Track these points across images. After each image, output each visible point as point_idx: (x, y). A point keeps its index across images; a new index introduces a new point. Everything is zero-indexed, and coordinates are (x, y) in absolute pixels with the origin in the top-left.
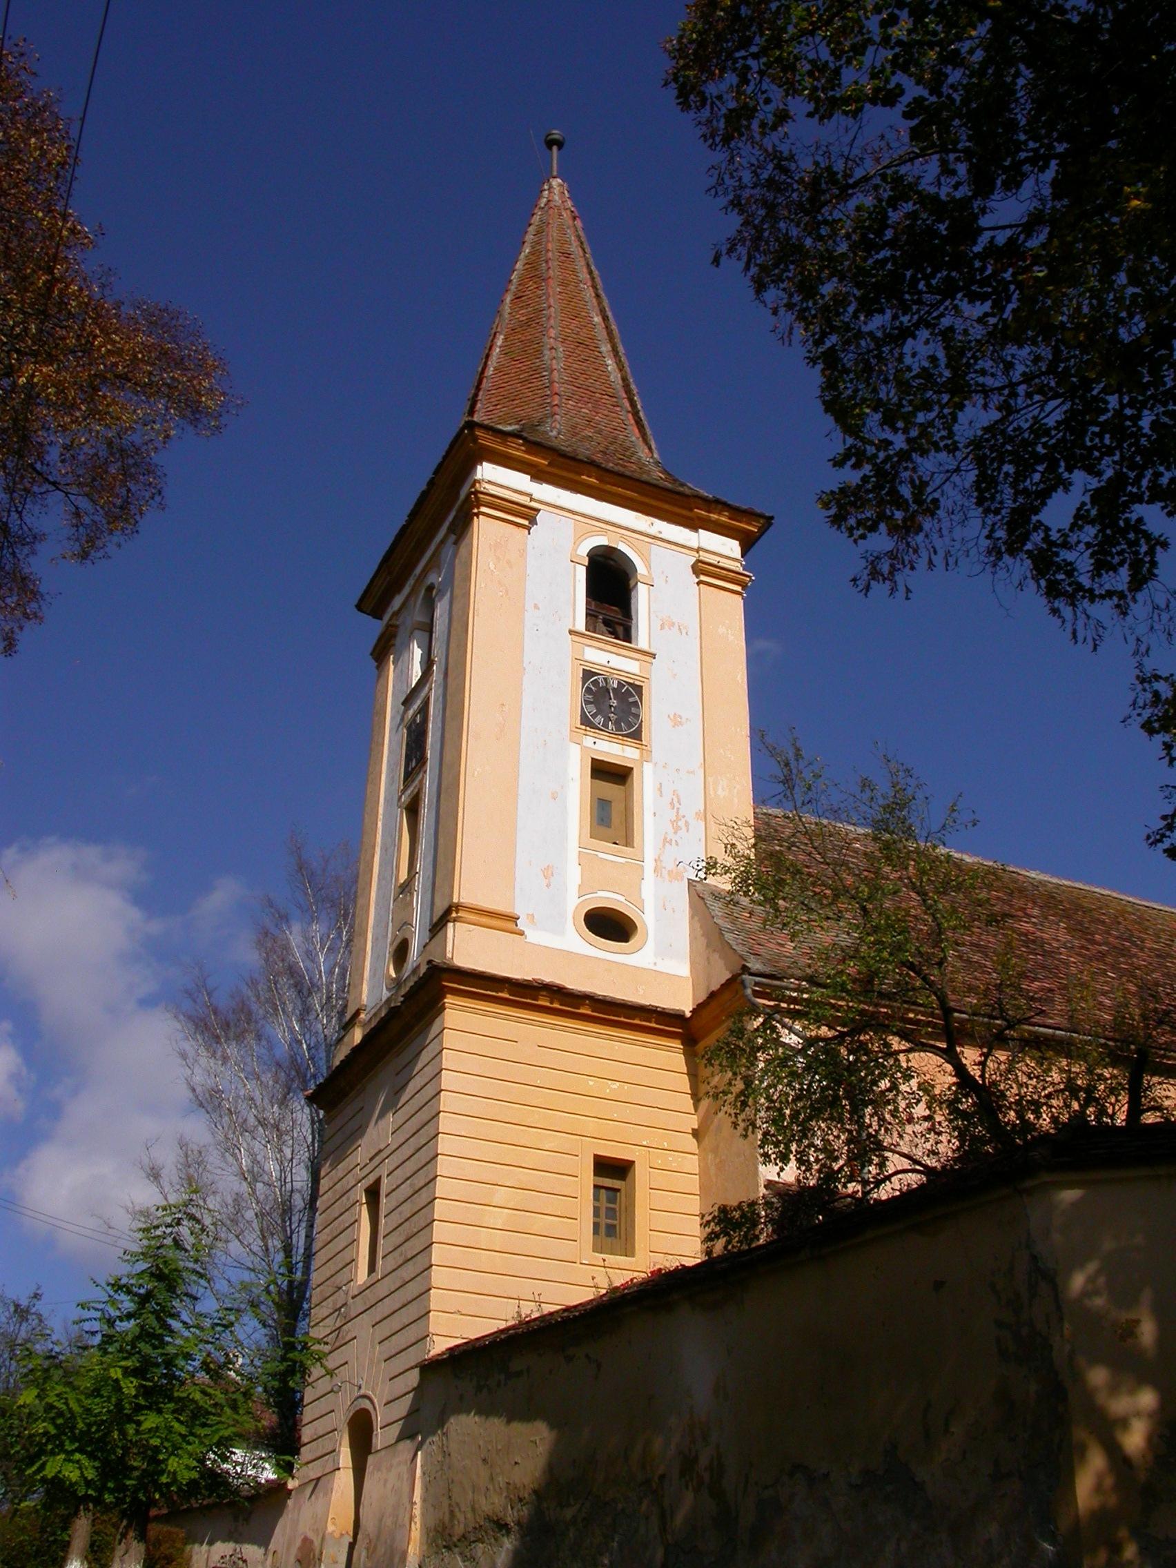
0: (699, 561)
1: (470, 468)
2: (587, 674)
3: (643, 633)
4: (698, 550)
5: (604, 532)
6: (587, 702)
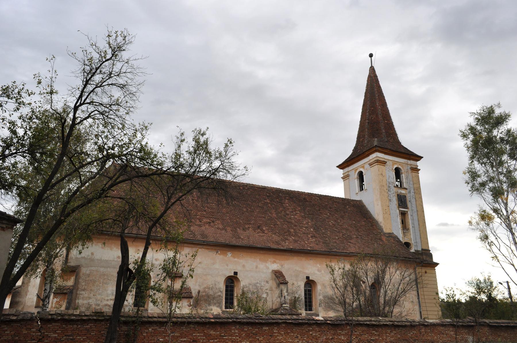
2: (398, 195)
3: (405, 185)
4: (411, 165)
5: (396, 164)
6: (398, 201)
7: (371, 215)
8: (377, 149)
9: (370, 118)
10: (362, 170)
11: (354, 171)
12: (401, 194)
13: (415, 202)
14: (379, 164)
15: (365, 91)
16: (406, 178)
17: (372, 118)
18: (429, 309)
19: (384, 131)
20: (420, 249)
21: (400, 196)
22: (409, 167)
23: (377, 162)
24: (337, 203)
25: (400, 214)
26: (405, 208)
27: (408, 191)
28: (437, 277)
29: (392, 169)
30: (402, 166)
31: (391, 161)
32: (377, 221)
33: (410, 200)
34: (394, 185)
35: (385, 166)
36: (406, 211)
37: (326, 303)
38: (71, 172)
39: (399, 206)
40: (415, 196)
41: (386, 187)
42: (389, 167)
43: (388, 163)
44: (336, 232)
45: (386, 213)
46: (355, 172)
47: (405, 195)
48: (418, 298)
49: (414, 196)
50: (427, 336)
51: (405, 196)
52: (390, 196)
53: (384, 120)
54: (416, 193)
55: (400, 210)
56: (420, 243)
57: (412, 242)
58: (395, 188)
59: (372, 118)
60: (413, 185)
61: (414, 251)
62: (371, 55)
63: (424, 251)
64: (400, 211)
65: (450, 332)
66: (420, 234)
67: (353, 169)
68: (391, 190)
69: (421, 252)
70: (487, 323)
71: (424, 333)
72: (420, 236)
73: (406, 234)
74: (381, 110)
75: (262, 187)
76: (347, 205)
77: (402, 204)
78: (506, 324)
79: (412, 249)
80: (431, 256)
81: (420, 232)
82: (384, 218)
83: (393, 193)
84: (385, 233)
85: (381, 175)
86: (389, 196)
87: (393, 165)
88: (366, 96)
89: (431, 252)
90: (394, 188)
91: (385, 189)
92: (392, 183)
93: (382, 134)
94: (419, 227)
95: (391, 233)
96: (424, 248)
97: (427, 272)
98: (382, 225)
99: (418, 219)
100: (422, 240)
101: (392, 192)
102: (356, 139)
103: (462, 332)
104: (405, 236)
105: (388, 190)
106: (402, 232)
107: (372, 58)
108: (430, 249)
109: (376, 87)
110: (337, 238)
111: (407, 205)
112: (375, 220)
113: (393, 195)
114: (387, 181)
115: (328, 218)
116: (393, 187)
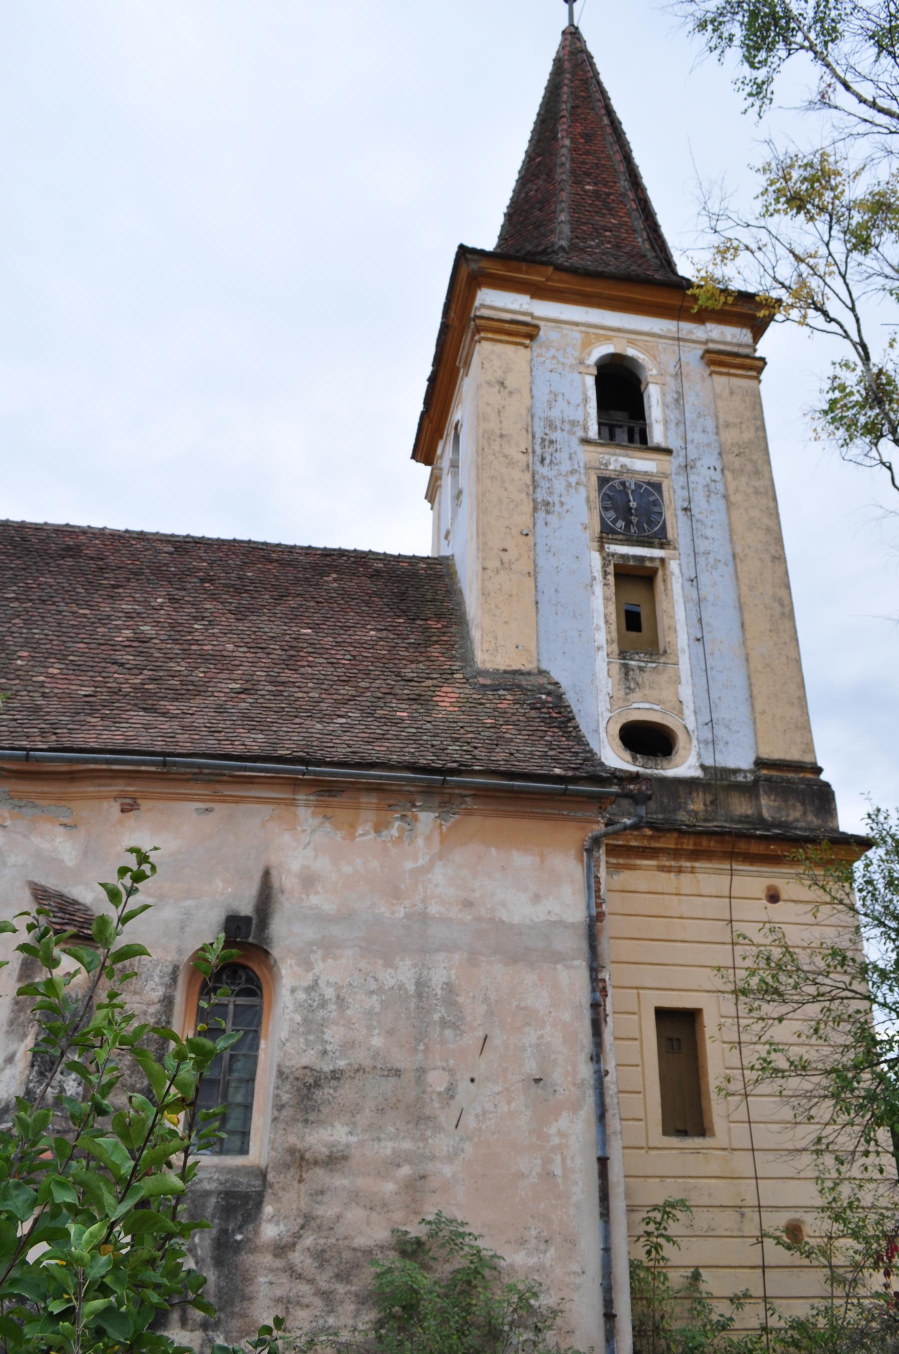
0: (708, 351)
1: (472, 297)
2: (603, 481)
3: (657, 435)
4: (706, 342)
5: (608, 339)
6: (606, 509)
8: (474, 266)
12: (624, 477)
14: (490, 335)
16: (669, 399)
21: (616, 483)
22: (699, 351)
25: (605, 574)
26: (650, 545)
29: (581, 362)
30: (646, 350)
31: (577, 324)
34: (580, 433)
35: (526, 347)
36: (652, 559)
38: (811, 862)
39: (607, 533)
47: (655, 479)
48: (597, 1057)
49: (720, 487)
51: (658, 487)
52: (544, 484)
54: (733, 472)
55: (613, 555)
60: (717, 434)
61: (699, 773)
63: (774, 773)
64: (606, 558)
66: (749, 678)
68: (563, 456)
69: (750, 777)
72: (750, 685)
73: (645, 678)
76: (335, 572)
77: (629, 523)
79: (676, 758)
81: (748, 667)
83: (573, 472)
84: (485, 673)
87: (587, 344)
89: (823, 777)
91: (514, 452)
92: (574, 423)
94: (744, 643)
95: (529, 673)
97: (784, 896)
99: (739, 597)
100: (759, 707)
101: (566, 467)
106: (616, 668)
111: (664, 528)
114: (539, 413)
116: (575, 442)
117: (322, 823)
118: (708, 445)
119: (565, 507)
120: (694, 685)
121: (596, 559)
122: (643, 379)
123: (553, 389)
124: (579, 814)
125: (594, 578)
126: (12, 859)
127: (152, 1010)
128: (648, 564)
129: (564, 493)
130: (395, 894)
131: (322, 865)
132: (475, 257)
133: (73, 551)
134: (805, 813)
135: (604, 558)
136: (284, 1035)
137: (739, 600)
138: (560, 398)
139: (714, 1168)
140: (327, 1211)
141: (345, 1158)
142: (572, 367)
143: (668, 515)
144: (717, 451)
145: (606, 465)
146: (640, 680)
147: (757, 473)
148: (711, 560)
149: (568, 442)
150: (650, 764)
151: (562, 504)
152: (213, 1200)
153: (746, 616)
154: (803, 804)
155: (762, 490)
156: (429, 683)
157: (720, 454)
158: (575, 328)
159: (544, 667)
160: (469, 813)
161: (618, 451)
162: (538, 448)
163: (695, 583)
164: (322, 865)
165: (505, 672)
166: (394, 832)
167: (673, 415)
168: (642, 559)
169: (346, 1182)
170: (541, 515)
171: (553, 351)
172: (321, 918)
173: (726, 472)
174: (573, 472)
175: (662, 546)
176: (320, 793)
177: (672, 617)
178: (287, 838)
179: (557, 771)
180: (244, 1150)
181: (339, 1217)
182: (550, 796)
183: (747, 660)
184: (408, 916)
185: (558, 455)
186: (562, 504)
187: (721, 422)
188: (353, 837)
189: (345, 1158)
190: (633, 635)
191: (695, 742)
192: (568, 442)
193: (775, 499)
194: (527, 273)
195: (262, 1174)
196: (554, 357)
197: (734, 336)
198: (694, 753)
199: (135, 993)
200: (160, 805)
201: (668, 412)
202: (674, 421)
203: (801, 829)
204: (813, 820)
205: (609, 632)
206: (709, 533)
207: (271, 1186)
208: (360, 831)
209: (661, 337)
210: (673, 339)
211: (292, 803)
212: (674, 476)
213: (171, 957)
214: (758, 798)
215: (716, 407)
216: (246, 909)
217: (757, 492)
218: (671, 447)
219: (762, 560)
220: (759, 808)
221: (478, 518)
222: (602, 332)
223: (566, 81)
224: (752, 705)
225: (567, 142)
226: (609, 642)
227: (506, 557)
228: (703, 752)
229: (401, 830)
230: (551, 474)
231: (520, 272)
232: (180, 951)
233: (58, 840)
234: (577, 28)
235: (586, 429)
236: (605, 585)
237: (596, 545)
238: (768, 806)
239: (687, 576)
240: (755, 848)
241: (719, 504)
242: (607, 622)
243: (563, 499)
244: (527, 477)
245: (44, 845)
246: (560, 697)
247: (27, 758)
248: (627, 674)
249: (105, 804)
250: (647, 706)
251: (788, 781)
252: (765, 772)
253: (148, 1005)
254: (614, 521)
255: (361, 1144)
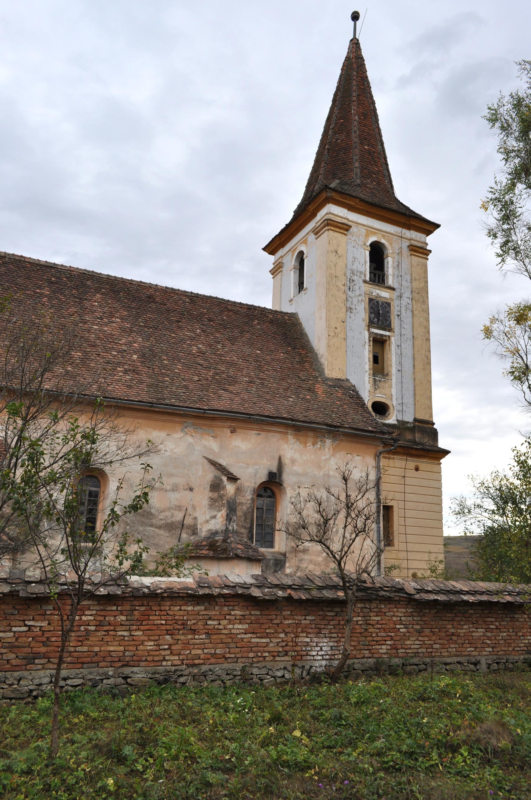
2: (371, 300)
3: (390, 281)
4: (410, 240)
5: (375, 233)
6: (371, 313)
7: (308, 341)
8: (329, 194)
9: (334, 140)
10: (303, 248)
11: (290, 254)
12: (378, 299)
13: (410, 319)
14: (332, 228)
15: (334, 90)
16: (395, 265)
17: (337, 140)
18: (410, 547)
19: (357, 164)
20: (409, 418)
22: (407, 243)
23: (328, 225)
24: (231, 313)
25: (370, 341)
26: (385, 330)
27: (396, 294)
28: (443, 481)
30: (388, 241)
31: (364, 225)
32: (316, 354)
33: (399, 313)
34: (363, 278)
35: (346, 235)
36: (386, 336)
37: (128, 524)
39: (371, 324)
40: (412, 305)
41: (343, 280)
42: (357, 239)
43: (354, 229)
44: (200, 367)
45: (336, 335)
46: (293, 255)
47: (389, 301)
49: (410, 306)
50: (107, 638)
51: (389, 304)
52: (350, 299)
53: (362, 143)
54: (416, 300)
55: (373, 333)
56: (412, 407)
57: (393, 403)
58: (367, 285)
59: (337, 140)
61: (396, 423)
62: (355, 17)
64: (370, 333)
65: (230, 622)
66: (414, 387)
67: (290, 250)
68: (356, 287)
69: (412, 425)
70: (406, 593)
71: (93, 628)
72: (415, 390)
73: (381, 384)
74: (359, 123)
75: (46, 264)
76: (256, 319)
77: (379, 320)
78: (484, 598)
79: (389, 417)
80: (434, 434)
81: (414, 383)
82: (329, 346)
83: (360, 295)
84: (328, 379)
85: (335, 253)
86: (347, 300)
87: (367, 236)
88: (334, 101)
89: (435, 426)
90: (363, 285)
91: (340, 284)
92: (361, 273)
93: (352, 170)
94: (414, 373)
95: (343, 380)
96: (421, 416)
97: (420, 468)
98: (323, 360)
99: (414, 354)
100: (417, 399)
101: (357, 293)
102: (305, 189)
103: (289, 625)
104: (376, 389)
105: (347, 288)
106: (371, 380)
107: (357, 22)
108: (434, 422)
109: (355, 77)
110: (196, 378)
112: (314, 351)
113: (360, 298)
114: (349, 267)
115: (192, 339)
116: (361, 281)
117: (296, 442)
118: (408, 287)
119: (357, 311)
120: (397, 389)
121: (367, 334)
122: (385, 253)
123: (354, 255)
124: (375, 443)
125: (366, 342)
126: (197, 448)
127: (248, 502)
128: (384, 338)
129: (357, 304)
130: (320, 467)
131: (297, 456)
132: (330, 191)
133: (151, 298)
134: (429, 440)
135: (369, 334)
136: (289, 512)
137: (414, 356)
138: (356, 260)
139: (393, 556)
140: (304, 565)
141: (308, 550)
142: (361, 245)
143: (392, 317)
144: (410, 291)
145: (372, 293)
146: (379, 385)
147: (424, 302)
148: (405, 338)
149: (358, 280)
150: (381, 418)
151: (356, 309)
152: (272, 561)
153: (416, 362)
154: (429, 437)
155: (425, 310)
156: (310, 382)
157: (411, 292)
158: (363, 227)
159: (348, 378)
160: (342, 441)
161: (376, 287)
162: (348, 283)
163: (400, 347)
164: (297, 456)
165: (336, 379)
166: (319, 446)
167: (396, 273)
168: (382, 335)
169: (308, 557)
170: (349, 313)
171: (354, 238)
172: (297, 474)
173: (413, 301)
174: (360, 295)
175: (389, 331)
176: (295, 430)
177: (391, 361)
178: (285, 446)
179: (370, 428)
180: (272, 547)
181: (307, 567)
182: (367, 437)
183: (414, 380)
184: (324, 475)
185: (355, 287)
186: (356, 309)
187: (413, 278)
188: (306, 447)
189: (308, 550)
190: (376, 365)
191: (395, 411)
192: (358, 280)
193: (429, 314)
194: (348, 201)
195: (284, 555)
196: (355, 240)
197: (420, 238)
198: (395, 415)
199: (243, 497)
200: (243, 431)
201: (395, 271)
202: (396, 276)
203: (427, 446)
204: (431, 442)
205: (370, 365)
206: (405, 326)
207: (288, 558)
208: (308, 445)
209: (394, 235)
210: (399, 236)
211: (286, 433)
212: (395, 301)
213: (253, 485)
214: (414, 433)
215: (412, 271)
216: (275, 470)
217: (423, 311)
218: (395, 287)
219: (422, 340)
220: (415, 437)
221: (326, 313)
222: (373, 230)
223: (355, 77)
224: (415, 398)
225: (357, 118)
226: (370, 369)
227: (337, 331)
228: (398, 415)
229: (321, 445)
230: (352, 295)
231: (346, 199)
232: (255, 483)
233: (211, 442)
234: (358, 40)
235: (365, 276)
236: (369, 345)
237: (367, 328)
238: (418, 436)
239: (397, 344)
240: (414, 452)
241: (409, 314)
242: (369, 361)
243: (356, 307)
244: (344, 297)
245: (207, 444)
246: (357, 392)
247: (204, 413)
248: (375, 383)
249: (225, 430)
250: (381, 395)
251: (424, 428)
252: (417, 424)
253: (247, 501)
254: (374, 319)
255: (312, 546)
